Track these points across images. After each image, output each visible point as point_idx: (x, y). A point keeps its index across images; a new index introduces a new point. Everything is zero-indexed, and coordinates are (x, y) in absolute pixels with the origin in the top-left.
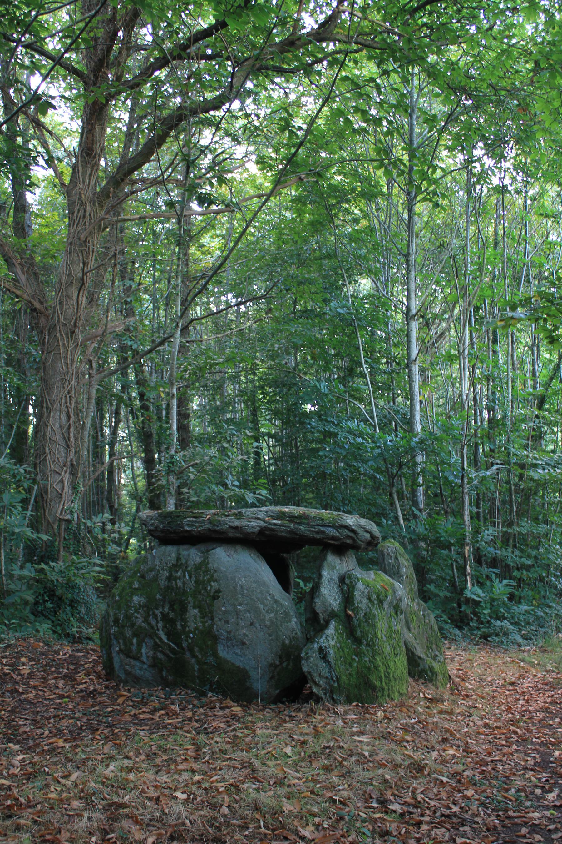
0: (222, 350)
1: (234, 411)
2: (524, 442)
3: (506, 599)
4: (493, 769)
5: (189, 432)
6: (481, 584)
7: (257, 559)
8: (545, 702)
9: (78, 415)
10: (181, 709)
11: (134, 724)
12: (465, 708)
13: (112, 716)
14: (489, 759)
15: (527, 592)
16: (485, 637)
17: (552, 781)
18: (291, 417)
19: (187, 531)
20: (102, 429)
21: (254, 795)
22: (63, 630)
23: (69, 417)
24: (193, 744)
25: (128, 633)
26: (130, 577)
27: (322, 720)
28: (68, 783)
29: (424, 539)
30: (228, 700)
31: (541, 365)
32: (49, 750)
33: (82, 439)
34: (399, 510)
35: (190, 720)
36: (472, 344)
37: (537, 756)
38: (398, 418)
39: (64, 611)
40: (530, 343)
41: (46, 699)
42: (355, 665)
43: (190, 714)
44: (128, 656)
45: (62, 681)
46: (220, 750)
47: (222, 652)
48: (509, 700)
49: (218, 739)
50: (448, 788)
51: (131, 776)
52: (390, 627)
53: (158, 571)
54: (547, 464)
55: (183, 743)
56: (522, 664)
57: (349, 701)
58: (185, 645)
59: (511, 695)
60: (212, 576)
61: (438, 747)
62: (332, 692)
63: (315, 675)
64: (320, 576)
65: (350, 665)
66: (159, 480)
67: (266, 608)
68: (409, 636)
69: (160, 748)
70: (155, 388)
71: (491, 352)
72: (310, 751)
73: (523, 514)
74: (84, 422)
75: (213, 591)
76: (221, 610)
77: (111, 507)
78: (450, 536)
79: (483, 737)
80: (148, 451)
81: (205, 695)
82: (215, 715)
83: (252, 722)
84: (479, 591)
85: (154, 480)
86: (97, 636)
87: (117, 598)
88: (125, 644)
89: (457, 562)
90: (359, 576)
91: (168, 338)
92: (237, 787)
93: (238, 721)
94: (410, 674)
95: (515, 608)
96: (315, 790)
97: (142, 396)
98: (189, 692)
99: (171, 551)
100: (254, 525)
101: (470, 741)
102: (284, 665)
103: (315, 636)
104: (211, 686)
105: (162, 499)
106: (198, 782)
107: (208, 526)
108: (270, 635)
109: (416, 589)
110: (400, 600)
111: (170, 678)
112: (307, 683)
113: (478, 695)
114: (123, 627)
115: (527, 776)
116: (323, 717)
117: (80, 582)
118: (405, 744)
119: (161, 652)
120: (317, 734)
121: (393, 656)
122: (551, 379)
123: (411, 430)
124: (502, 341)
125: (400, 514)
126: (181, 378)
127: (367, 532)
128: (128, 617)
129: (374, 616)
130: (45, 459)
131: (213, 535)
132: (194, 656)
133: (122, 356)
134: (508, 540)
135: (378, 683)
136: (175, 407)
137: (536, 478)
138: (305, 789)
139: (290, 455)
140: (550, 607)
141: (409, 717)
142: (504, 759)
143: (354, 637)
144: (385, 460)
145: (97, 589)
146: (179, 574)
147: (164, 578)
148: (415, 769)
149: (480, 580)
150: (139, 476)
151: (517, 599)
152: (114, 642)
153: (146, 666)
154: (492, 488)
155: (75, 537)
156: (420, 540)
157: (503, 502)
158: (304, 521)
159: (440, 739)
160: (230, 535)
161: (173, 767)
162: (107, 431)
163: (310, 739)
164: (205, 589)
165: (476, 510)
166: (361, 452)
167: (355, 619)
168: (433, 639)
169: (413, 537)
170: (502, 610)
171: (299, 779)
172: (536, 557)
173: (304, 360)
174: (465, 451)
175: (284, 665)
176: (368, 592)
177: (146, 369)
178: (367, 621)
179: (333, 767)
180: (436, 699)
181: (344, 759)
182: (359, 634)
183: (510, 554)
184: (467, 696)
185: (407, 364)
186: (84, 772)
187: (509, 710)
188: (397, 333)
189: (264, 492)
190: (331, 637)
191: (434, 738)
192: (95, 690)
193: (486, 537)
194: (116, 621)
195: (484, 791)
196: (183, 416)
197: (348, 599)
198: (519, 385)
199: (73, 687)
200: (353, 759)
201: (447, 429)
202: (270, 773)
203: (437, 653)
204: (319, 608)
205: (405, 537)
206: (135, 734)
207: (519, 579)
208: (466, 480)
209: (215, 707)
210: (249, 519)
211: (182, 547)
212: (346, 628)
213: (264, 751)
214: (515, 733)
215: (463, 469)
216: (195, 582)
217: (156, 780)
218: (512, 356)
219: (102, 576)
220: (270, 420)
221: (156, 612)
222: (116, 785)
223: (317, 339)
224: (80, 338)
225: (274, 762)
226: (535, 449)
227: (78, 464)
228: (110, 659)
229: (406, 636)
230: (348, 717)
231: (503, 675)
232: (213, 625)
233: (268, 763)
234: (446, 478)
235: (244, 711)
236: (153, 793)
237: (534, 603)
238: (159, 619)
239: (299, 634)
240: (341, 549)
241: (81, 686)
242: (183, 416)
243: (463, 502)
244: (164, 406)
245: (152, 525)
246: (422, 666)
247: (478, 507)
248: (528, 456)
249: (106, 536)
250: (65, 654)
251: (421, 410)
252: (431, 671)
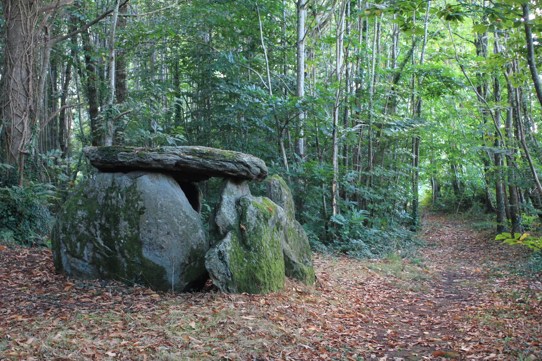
0: (153, 25)
1: (161, 75)
2: (382, 108)
3: (361, 224)
4: (342, 341)
5: (125, 89)
6: (343, 213)
7: (174, 185)
8: (384, 297)
9: (36, 72)
10: (113, 295)
11: (77, 305)
12: (325, 299)
13: (60, 300)
14: (340, 334)
15: (377, 220)
16: (344, 251)
17: (383, 350)
18: (205, 81)
19: (121, 162)
20: (55, 84)
21: (166, 354)
22: (23, 238)
23: (28, 72)
24: (122, 320)
25: (74, 239)
26: (75, 196)
27: (219, 304)
28: (25, 346)
29: (303, 178)
30: (150, 290)
31: (399, 51)
32: (11, 323)
33: (38, 90)
34: (285, 155)
35: (120, 303)
36: (347, 30)
37: (375, 333)
38: (287, 85)
39: (24, 224)
40: (391, 33)
41: (8, 287)
42: (245, 265)
43: (120, 299)
44: (73, 256)
45: (22, 275)
46: (142, 324)
47: (146, 254)
48: (358, 295)
49: (141, 316)
50: (309, 353)
51: (74, 341)
52: (272, 239)
53: (98, 192)
54: (399, 126)
55: (114, 318)
56: (370, 270)
57: (240, 291)
58: (117, 248)
59: (360, 291)
60: (139, 197)
61: (303, 325)
62: (227, 284)
63: (215, 271)
64: (221, 199)
65: (242, 265)
66: (100, 126)
67: (180, 222)
68: (286, 247)
69: (96, 322)
70: (98, 54)
71: (361, 38)
72: (209, 326)
73: (377, 163)
74: (40, 77)
75: (139, 208)
76: (145, 223)
77: (62, 147)
78: (322, 175)
79: (337, 319)
80: (92, 103)
81: (132, 286)
82: (139, 300)
83: (167, 305)
84: (342, 218)
85: (96, 125)
86: (49, 242)
87: (65, 212)
88: (71, 247)
89: (326, 196)
90: (251, 200)
91: (109, 12)
92: (153, 349)
93: (156, 304)
94: (286, 274)
95: (368, 231)
96: (212, 352)
97: (87, 59)
98: (120, 283)
99: (108, 178)
100: (172, 159)
101: (327, 322)
102: (192, 264)
103: (216, 243)
104: (137, 279)
105: (103, 141)
106: (125, 345)
107: (137, 159)
108: (182, 242)
109: (294, 212)
110: (281, 219)
111: (105, 273)
112: (209, 278)
113: (336, 291)
114: (70, 234)
115: (366, 346)
116: (220, 302)
117: (37, 202)
118: (280, 322)
119: (99, 253)
120: (215, 313)
121: (274, 260)
122: (406, 61)
123: (297, 94)
124: (369, 31)
125: (285, 158)
126: (119, 46)
127: (258, 167)
128: (73, 227)
129: (261, 230)
130: (8, 105)
131: (141, 166)
132: (124, 256)
133: (72, 26)
134: (365, 181)
135: (262, 279)
136: (114, 68)
137: (389, 135)
138: (204, 351)
139: (204, 110)
140: (393, 231)
141: (284, 304)
142: (351, 334)
143: (245, 245)
144: (275, 116)
145: (50, 208)
146: (114, 194)
147: (102, 197)
148: (286, 339)
149: (343, 210)
150: (85, 123)
151: (370, 225)
152: (63, 245)
153: (87, 264)
154: (356, 141)
155: (33, 167)
156: (299, 178)
157: (364, 153)
158: (210, 157)
159: (306, 319)
160: (154, 166)
161: (106, 335)
162: (60, 87)
163: (209, 317)
164: (134, 206)
165: (342, 157)
166: (257, 109)
167: (246, 232)
168: (305, 249)
169: (294, 175)
170: (358, 232)
171: (200, 344)
172: (385, 195)
173: (217, 36)
174: (337, 112)
175: (192, 264)
176: (257, 212)
177: (92, 38)
178: (255, 234)
179: (226, 337)
180: (304, 292)
181: (234, 332)
182: (249, 243)
183: (366, 191)
184: (328, 291)
185: (296, 44)
186: (38, 338)
187: (357, 301)
188: (290, 19)
189: (182, 136)
190: (228, 244)
191: (301, 319)
192: (47, 281)
193: (349, 177)
194: (64, 229)
195: (335, 355)
196: (120, 77)
197: (241, 216)
198: (381, 63)
199: (30, 278)
200: (241, 331)
201: (324, 95)
202: (178, 339)
203: (307, 260)
204: (220, 223)
205: (288, 175)
206: (78, 312)
207: (372, 210)
208: (336, 134)
209: (139, 294)
210: (169, 154)
211: (116, 175)
212: (239, 238)
213: (176, 325)
214: (361, 317)
215: (334, 125)
216: (126, 201)
217: (92, 343)
218: (377, 41)
219: (54, 197)
220: (189, 83)
221: (96, 223)
222: (62, 347)
223: (227, 20)
224: (38, 8)
225: (182, 333)
226: (390, 114)
227: (36, 110)
228: (59, 258)
229: (285, 247)
230: (239, 302)
231: (355, 277)
232: (139, 233)
233: (178, 333)
234: (321, 132)
235: (161, 297)
236: (90, 352)
237: (382, 228)
238: (98, 228)
239: (204, 242)
240: (237, 180)
241: (37, 278)
242: (120, 77)
243: (333, 151)
244: (106, 68)
245: (93, 157)
246: (295, 269)
247: (344, 155)
248: (384, 119)
249: (58, 167)
250: (24, 255)
251: (306, 79)
252: (302, 272)
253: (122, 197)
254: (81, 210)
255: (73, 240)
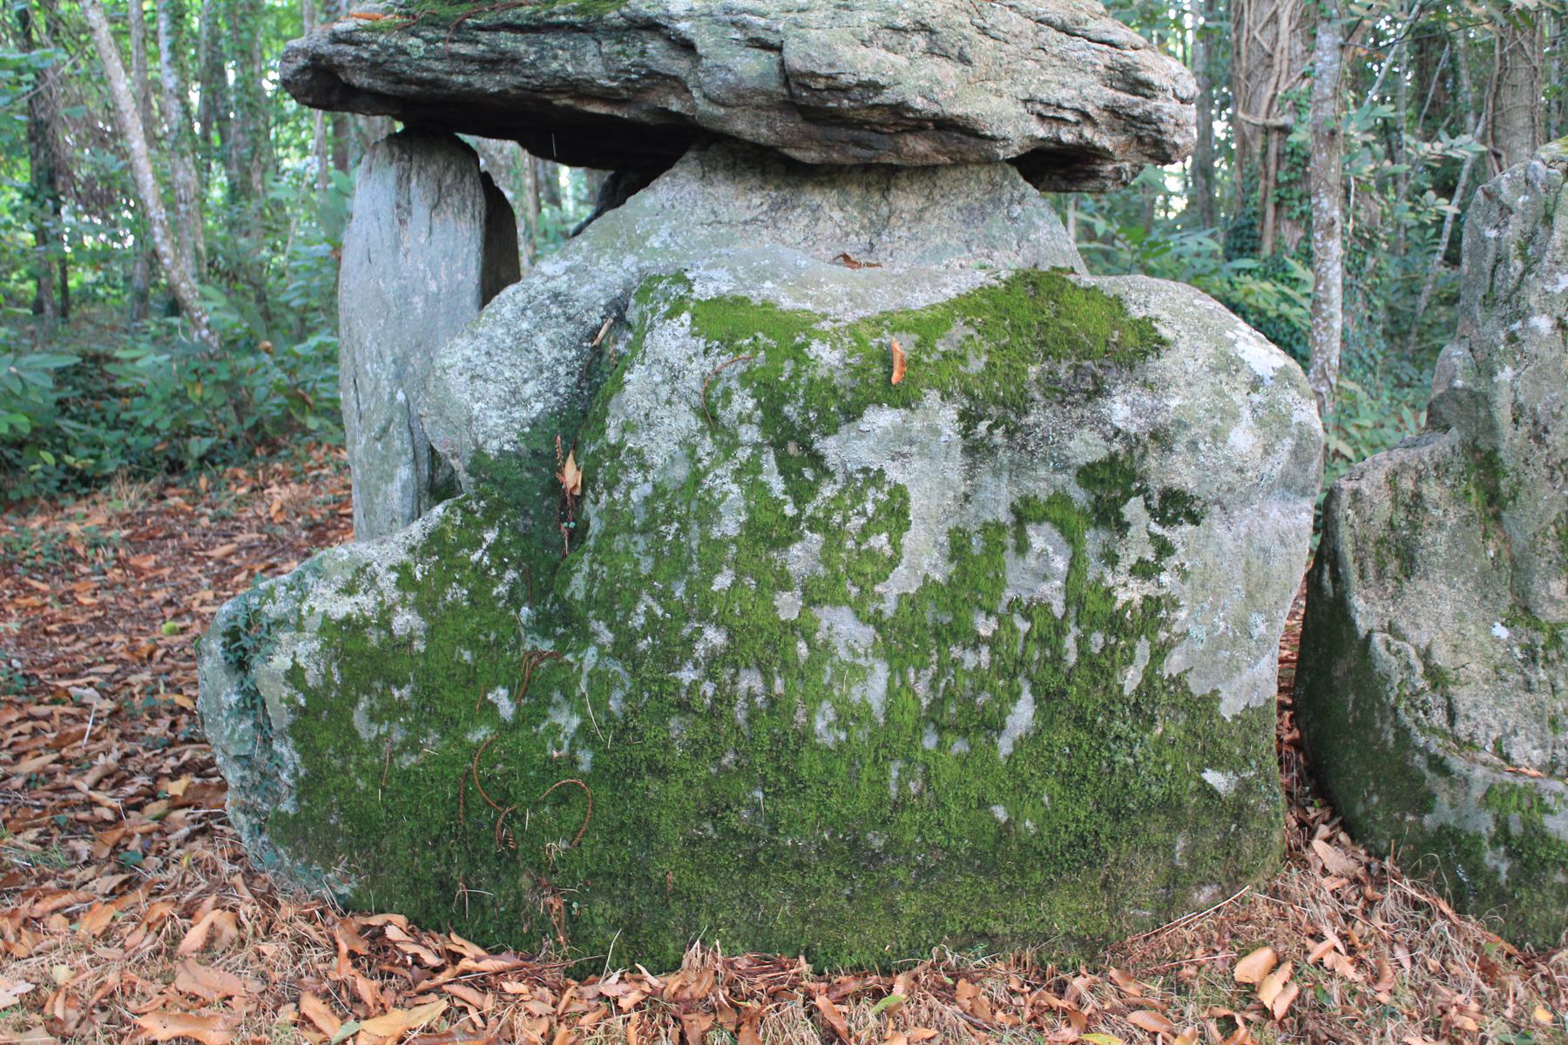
246: (1443, 813)
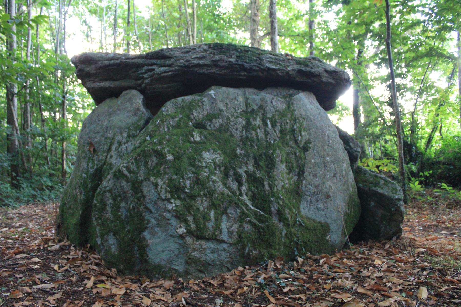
25: (202, 204)
75: (303, 142)
88: (196, 221)
114: (193, 197)
147: (240, 127)
216: (281, 132)
253: (274, 125)
254: (209, 151)
255: (201, 209)
